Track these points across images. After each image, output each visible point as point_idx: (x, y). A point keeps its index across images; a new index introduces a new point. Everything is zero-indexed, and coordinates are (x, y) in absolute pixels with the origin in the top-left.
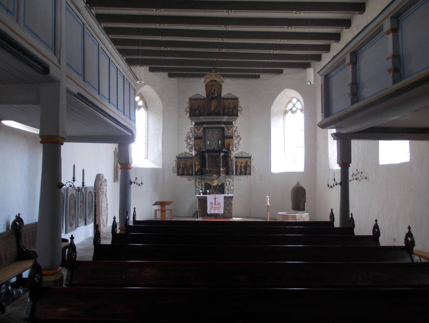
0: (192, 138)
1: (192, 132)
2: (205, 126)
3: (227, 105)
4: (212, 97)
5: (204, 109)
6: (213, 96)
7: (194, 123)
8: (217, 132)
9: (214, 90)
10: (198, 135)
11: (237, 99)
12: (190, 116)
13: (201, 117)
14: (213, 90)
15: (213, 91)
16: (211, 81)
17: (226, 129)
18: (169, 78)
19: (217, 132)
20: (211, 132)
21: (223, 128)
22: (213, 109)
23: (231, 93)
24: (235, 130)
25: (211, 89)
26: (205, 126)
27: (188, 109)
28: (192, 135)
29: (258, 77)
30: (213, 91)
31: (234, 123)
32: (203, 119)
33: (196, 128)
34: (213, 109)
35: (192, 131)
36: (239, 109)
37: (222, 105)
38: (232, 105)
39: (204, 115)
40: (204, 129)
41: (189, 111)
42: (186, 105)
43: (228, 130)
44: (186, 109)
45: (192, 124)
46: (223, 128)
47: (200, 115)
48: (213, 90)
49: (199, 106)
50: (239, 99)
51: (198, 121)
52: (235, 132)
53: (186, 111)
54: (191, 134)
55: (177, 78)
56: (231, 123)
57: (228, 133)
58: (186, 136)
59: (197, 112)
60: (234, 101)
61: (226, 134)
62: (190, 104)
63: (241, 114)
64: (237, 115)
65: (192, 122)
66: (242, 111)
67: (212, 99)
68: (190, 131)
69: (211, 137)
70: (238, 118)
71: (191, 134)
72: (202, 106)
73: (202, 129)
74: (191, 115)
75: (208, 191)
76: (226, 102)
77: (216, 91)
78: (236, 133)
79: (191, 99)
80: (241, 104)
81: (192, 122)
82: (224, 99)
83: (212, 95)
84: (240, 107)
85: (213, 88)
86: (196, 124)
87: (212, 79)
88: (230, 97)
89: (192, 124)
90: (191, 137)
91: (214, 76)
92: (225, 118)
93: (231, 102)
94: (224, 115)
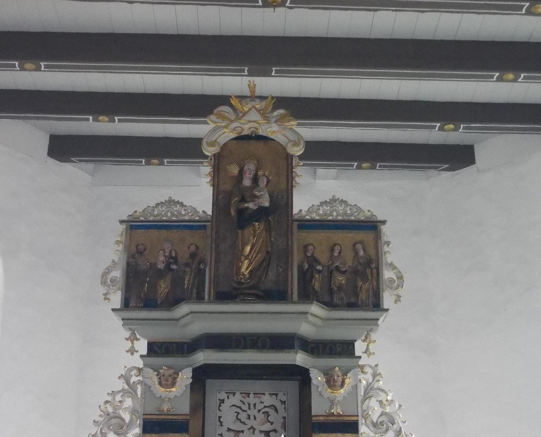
0: (130, 425)
1: (130, 391)
2: (203, 357)
3: (323, 256)
4: (241, 212)
5: (200, 273)
6: (251, 206)
7: (142, 346)
8: (268, 400)
9: (255, 180)
10: (165, 407)
11: (372, 226)
12: (126, 304)
13: (184, 309)
14: (252, 201)
15: (247, 182)
16: (240, 138)
17: (317, 378)
18: (52, 161)
19: (268, 400)
20: (236, 400)
21: (302, 376)
22: (245, 268)
23: (340, 196)
24: (369, 388)
25: (241, 172)
26: (203, 357)
27: (118, 274)
28: (133, 412)
29: (460, 157)
30: (247, 182)
31: (359, 347)
32: (195, 318)
33: (156, 369)
34: (245, 268)
35: (132, 387)
36: (387, 274)
37: (297, 258)
38: (348, 255)
39: (200, 299)
40: (202, 375)
41: (121, 283)
42: (111, 253)
43: (331, 383)
44: (105, 274)
45: (132, 351)
46: (302, 376)
47: (173, 302)
48: (252, 201)
49: (173, 259)
50: (384, 229)
51: (165, 333)
52: (367, 396)
53: (104, 283)
54: (129, 402)
55: (90, 166)
56: (346, 349)
57: (332, 403)
58: (96, 415)
59: (163, 287)
60: (360, 235)
61: (318, 408)
62: (127, 248)
63: (398, 299)
64: (377, 305)
65: (133, 338)
66: (400, 286)
67: (244, 219)
68: (121, 385)
69: (238, 427)
70: (384, 320)
71: (129, 402)
72: (193, 256)
73: (185, 377)
74: (132, 303)
75: (281, 270)
76: (319, 242)
77: (263, 182)
78: (373, 403)
79: (134, 226)
80: (398, 252)
81: (133, 338)
82: (307, 225)
83: (243, 200)
84: (392, 266)
85: (250, 167)
86: (155, 349)
87: (247, 128)
88: (337, 214)
89: (132, 351)
90: (127, 417)
91: (254, 116)
92: (312, 320)
93: (345, 238)
94: (307, 295)
